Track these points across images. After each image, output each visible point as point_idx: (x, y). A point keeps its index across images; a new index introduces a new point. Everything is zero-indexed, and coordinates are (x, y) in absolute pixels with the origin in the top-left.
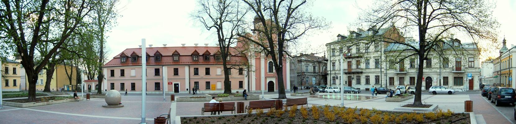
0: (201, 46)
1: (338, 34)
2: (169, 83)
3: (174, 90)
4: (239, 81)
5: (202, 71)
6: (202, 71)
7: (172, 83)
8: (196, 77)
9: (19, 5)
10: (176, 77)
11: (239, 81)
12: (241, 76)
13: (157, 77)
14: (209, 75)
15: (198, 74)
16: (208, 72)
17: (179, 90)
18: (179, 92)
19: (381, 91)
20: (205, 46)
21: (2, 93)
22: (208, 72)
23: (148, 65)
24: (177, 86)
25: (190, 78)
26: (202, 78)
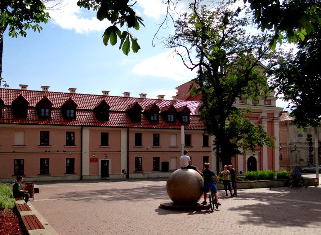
0: (114, 95)
1: (141, 46)
2: (91, 160)
3: (100, 174)
4: (41, 159)
5: (147, 140)
6: (147, 140)
7: (97, 160)
8: (139, 149)
9: (262, 51)
10: (104, 149)
11: (41, 159)
12: (205, 149)
13: (44, 149)
14: (108, 145)
15: (158, 145)
16: (156, 142)
17: (110, 173)
18: (110, 176)
19: (251, 197)
20: (69, 92)
21: (158, 170)
22: (156, 142)
23: (187, 129)
24: (106, 165)
25: (81, 152)
26: (147, 152)
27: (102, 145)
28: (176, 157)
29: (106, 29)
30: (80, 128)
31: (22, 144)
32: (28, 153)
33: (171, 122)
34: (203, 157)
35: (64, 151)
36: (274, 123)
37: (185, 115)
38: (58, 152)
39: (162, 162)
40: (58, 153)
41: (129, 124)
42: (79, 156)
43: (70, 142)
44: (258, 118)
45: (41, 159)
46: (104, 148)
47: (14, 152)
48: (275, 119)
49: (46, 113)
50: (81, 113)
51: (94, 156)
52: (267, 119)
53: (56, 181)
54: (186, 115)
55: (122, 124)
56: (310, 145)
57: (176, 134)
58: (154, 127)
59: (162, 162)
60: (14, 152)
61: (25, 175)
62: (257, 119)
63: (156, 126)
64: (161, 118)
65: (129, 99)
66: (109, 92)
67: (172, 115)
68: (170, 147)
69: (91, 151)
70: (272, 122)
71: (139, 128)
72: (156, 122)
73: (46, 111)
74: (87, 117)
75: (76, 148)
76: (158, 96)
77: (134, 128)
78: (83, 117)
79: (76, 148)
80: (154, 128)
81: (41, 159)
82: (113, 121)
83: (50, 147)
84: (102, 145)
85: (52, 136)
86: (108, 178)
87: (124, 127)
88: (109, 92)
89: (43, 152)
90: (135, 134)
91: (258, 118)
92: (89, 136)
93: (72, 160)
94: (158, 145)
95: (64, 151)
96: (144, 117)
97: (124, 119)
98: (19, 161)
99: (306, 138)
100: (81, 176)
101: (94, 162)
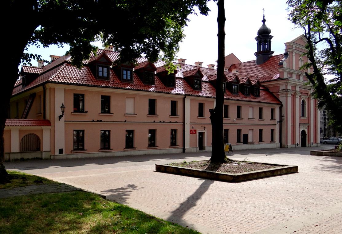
15: (109, 112)
27: (149, 114)
28: (253, 130)
29: (225, 20)
30: (183, 97)
31: (252, 118)
32: (77, 122)
33: (127, 80)
34: (178, 129)
35: (170, 122)
36: (296, 96)
37: (103, 67)
38: (170, 122)
39: (243, 134)
40: (93, 122)
41: (93, 81)
42: (181, 127)
43: (174, 112)
44: (308, 94)
45: (260, 130)
46: (250, 121)
47: (125, 121)
48: (297, 92)
49: (128, 76)
50: (72, 68)
51: (193, 127)
52: (292, 92)
53: (154, 155)
54: (105, 67)
55: (82, 80)
56: (325, 120)
57: (134, 98)
58: (103, 85)
59: (243, 134)
60: (125, 121)
61: (112, 149)
62: (306, 95)
63: (105, 84)
64: (113, 74)
65: (112, 53)
66: (185, 60)
67: (128, 71)
68: (125, 115)
69: (67, 120)
70: (294, 95)
71: (107, 87)
72: (105, 79)
73: (102, 72)
74: (82, 74)
75: (179, 119)
76: (195, 63)
77: (101, 87)
78: (68, 72)
79: (179, 119)
80: (150, 92)
81: (260, 130)
82: (68, 76)
83: (112, 116)
84: (149, 114)
85: (113, 103)
86: (204, 151)
87: (86, 84)
88: (202, 63)
89: (152, 122)
90: (149, 99)
91: (308, 94)
92: (189, 106)
93: (175, 131)
94: (109, 112)
95: (97, 120)
96: (88, 71)
97: (84, 74)
98: (78, 132)
99: (323, 113)
100: (184, 149)
101: (193, 134)
